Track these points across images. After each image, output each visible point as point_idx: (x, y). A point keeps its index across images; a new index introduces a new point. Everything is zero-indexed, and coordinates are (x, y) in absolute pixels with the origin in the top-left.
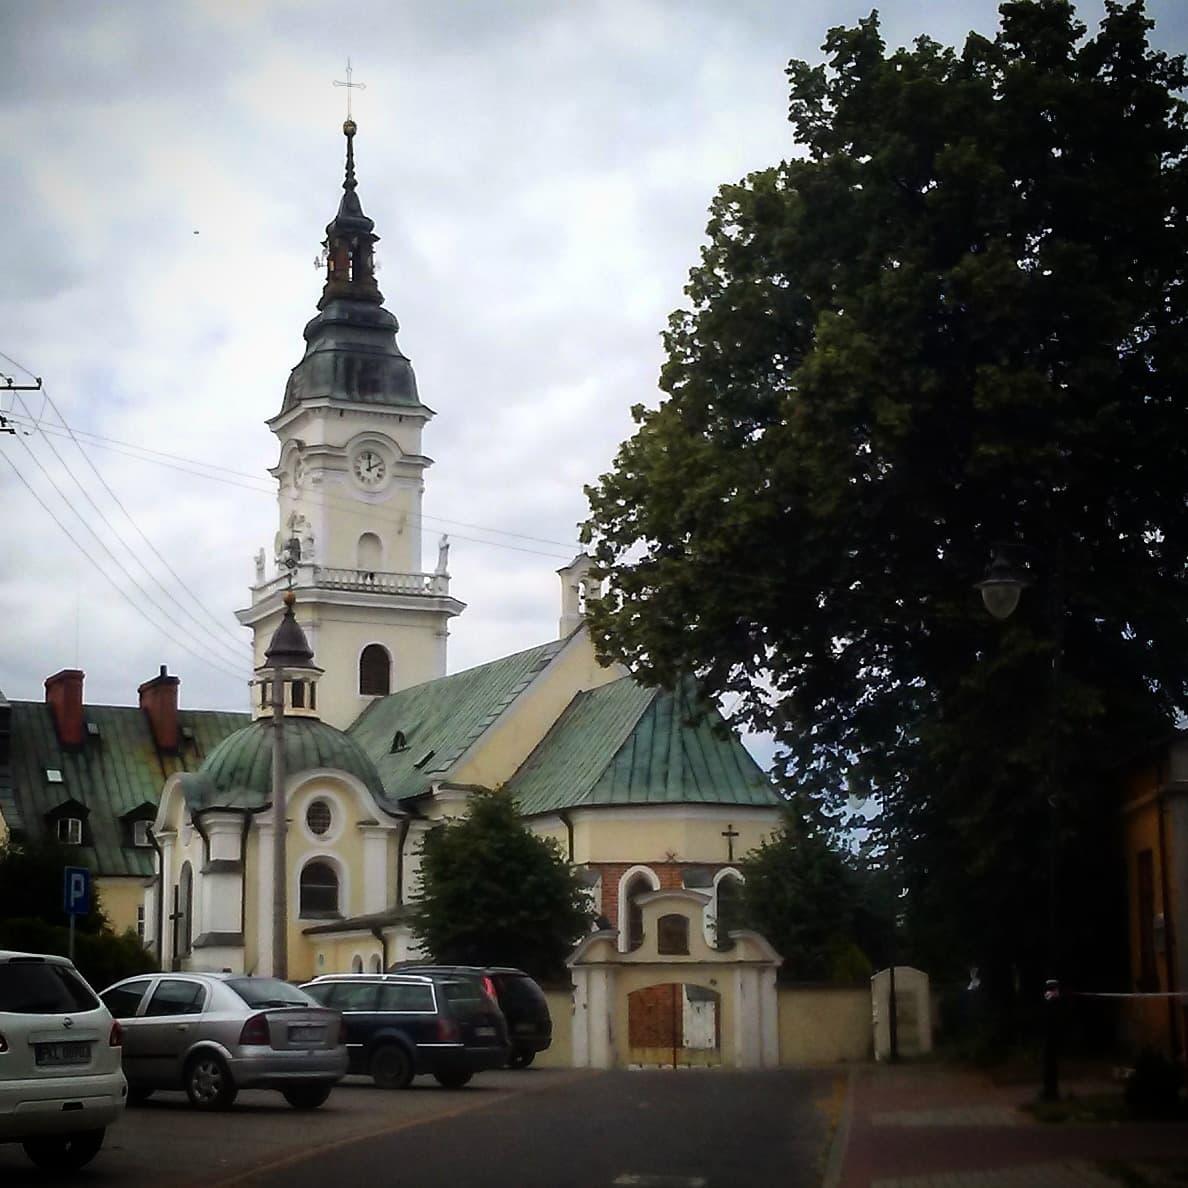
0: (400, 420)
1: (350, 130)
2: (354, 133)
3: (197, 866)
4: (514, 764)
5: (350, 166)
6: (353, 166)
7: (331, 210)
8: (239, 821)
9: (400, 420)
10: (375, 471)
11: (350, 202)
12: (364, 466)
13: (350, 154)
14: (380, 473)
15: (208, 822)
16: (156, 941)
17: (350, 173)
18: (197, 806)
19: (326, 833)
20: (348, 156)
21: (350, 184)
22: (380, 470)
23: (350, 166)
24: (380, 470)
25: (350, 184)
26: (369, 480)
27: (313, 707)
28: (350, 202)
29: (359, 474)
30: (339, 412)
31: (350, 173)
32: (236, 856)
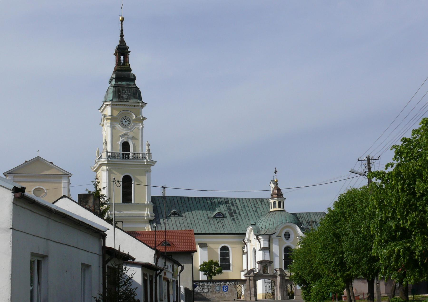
2: (123, 21)
3: (257, 249)
4: (11, 211)
5: (122, 31)
6: (123, 31)
7: (117, 43)
8: (267, 237)
10: (128, 122)
11: (122, 41)
12: (124, 121)
13: (122, 27)
14: (129, 123)
15: (259, 238)
16: (247, 269)
17: (122, 33)
18: (257, 233)
19: (289, 239)
20: (121, 27)
21: (122, 36)
22: (129, 122)
23: (122, 31)
24: (129, 122)
25: (122, 36)
26: (126, 125)
27: (284, 208)
28: (122, 41)
29: (122, 123)
30: (115, 105)
31: (122, 33)
32: (268, 246)
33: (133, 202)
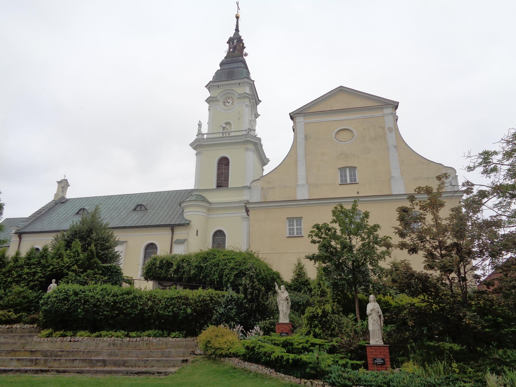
0: (218, 87)
1: (237, 18)
5: (237, 26)
9: (218, 87)
21: (237, 30)
23: (237, 26)
25: (237, 30)
26: (228, 106)
30: (217, 87)
33: (231, 185)
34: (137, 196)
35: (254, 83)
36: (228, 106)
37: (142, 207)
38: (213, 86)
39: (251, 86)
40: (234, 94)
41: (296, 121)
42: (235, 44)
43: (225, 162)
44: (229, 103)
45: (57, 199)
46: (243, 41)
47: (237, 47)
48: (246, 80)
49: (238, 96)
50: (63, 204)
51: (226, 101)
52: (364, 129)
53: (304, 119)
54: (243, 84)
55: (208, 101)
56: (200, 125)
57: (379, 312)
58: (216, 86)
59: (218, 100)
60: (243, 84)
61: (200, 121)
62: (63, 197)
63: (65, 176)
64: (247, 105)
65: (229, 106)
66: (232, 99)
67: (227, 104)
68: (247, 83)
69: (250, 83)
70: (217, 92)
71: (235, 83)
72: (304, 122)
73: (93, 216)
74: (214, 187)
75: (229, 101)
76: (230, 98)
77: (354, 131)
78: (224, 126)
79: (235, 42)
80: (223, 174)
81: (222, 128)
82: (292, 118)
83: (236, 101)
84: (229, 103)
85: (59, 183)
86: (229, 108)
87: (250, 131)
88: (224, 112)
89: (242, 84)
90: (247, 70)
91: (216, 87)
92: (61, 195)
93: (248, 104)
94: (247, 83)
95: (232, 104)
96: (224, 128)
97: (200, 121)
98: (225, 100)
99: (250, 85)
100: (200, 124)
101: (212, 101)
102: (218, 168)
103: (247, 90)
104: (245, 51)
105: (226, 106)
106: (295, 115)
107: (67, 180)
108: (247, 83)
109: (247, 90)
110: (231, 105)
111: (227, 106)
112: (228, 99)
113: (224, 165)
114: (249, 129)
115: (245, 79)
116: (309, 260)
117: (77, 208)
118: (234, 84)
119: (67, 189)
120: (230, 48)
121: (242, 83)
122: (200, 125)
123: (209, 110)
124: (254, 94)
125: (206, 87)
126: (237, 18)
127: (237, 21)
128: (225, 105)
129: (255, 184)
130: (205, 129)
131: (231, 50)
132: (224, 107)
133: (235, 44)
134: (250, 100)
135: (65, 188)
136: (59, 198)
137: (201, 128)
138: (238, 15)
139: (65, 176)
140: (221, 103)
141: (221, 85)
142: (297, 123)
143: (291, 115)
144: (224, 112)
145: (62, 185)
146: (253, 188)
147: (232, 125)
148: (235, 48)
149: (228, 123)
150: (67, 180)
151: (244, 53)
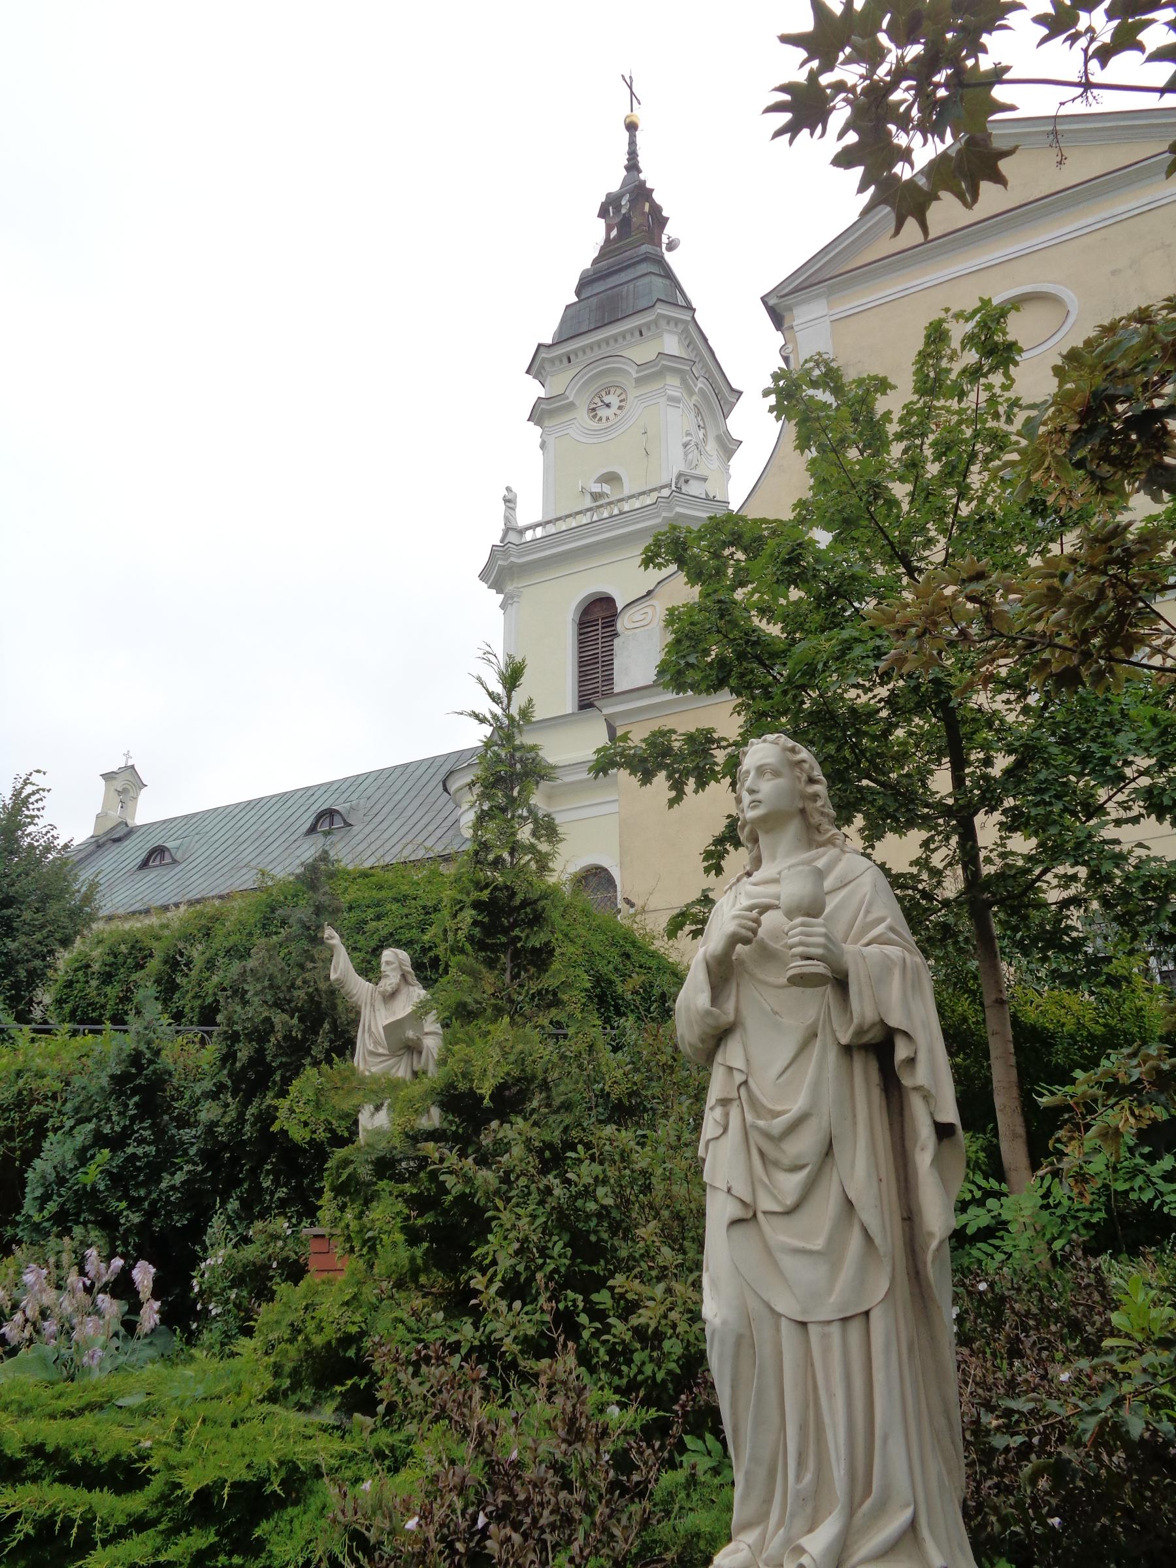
1: (632, 127)
5: (633, 154)
21: (633, 166)
23: (633, 154)
25: (633, 166)
26: (608, 419)
30: (565, 360)
34: (335, 787)
35: (693, 317)
36: (608, 419)
37: (337, 818)
38: (552, 361)
39: (685, 331)
40: (620, 369)
41: (795, 323)
42: (624, 211)
43: (603, 614)
44: (608, 405)
45: (101, 832)
46: (655, 195)
47: (634, 220)
48: (661, 309)
49: (638, 372)
50: (117, 844)
51: (600, 404)
52: (1113, 273)
53: (830, 308)
54: (653, 327)
55: (539, 414)
56: (510, 502)
57: (841, 983)
58: (559, 358)
59: (571, 406)
60: (653, 327)
61: (508, 489)
62: (121, 823)
63: (127, 755)
64: (672, 399)
65: (612, 417)
66: (619, 391)
67: (603, 413)
68: (669, 320)
69: (677, 322)
70: (561, 381)
71: (627, 331)
72: (827, 320)
73: (851, 1057)
74: (576, 710)
75: (607, 399)
76: (612, 390)
77: (1066, 294)
78: (596, 488)
79: (623, 203)
80: (600, 659)
81: (588, 497)
82: (778, 318)
83: (632, 393)
84: (608, 405)
85: (108, 777)
86: (610, 424)
87: (687, 482)
88: (595, 441)
89: (649, 329)
90: (668, 282)
91: (561, 361)
92: (116, 814)
93: (678, 394)
94: (668, 323)
95: (620, 408)
96: (595, 496)
97: (508, 489)
98: (597, 400)
99: (681, 327)
100: (509, 497)
101: (552, 413)
102: (580, 642)
103: (671, 344)
104: (670, 231)
105: (600, 419)
106: (789, 300)
107: (133, 767)
108: (668, 323)
109: (671, 344)
110: (618, 412)
111: (604, 420)
112: (603, 393)
113: (599, 627)
114: (680, 475)
115: (658, 305)
116: (628, 771)
117: (148, 846)
118: (623, 335)
119: (136, 798)
120: (609, 229)
121: (648, 325)
122: (510, 502)
123: (543, 446)
124: (699, 354)
125: (528, 372)
126: (632, 127)
127: (632, 143)
128: (595, 416)
129: (637, 617)
130: (530, 511)
131: (614, 233)
132: (594, 425)
133: (624, 211)
134: (684, 381)
135: (131, 794)
136: (110, 825)
137: (513, 509)
138: (634, 119)
139: (127, 755)
140: (582, 415)
141: (575, 352)
142: (796, 329)
143: (771, 302)
144: (595, 441)
145: (119, 784)
146: (630, 632)
147: (624, 480)
148: (625, 225)
149: (611, 478)
150: (133, 767)
151: (665, 239)
